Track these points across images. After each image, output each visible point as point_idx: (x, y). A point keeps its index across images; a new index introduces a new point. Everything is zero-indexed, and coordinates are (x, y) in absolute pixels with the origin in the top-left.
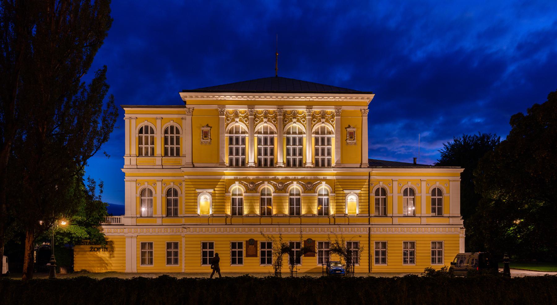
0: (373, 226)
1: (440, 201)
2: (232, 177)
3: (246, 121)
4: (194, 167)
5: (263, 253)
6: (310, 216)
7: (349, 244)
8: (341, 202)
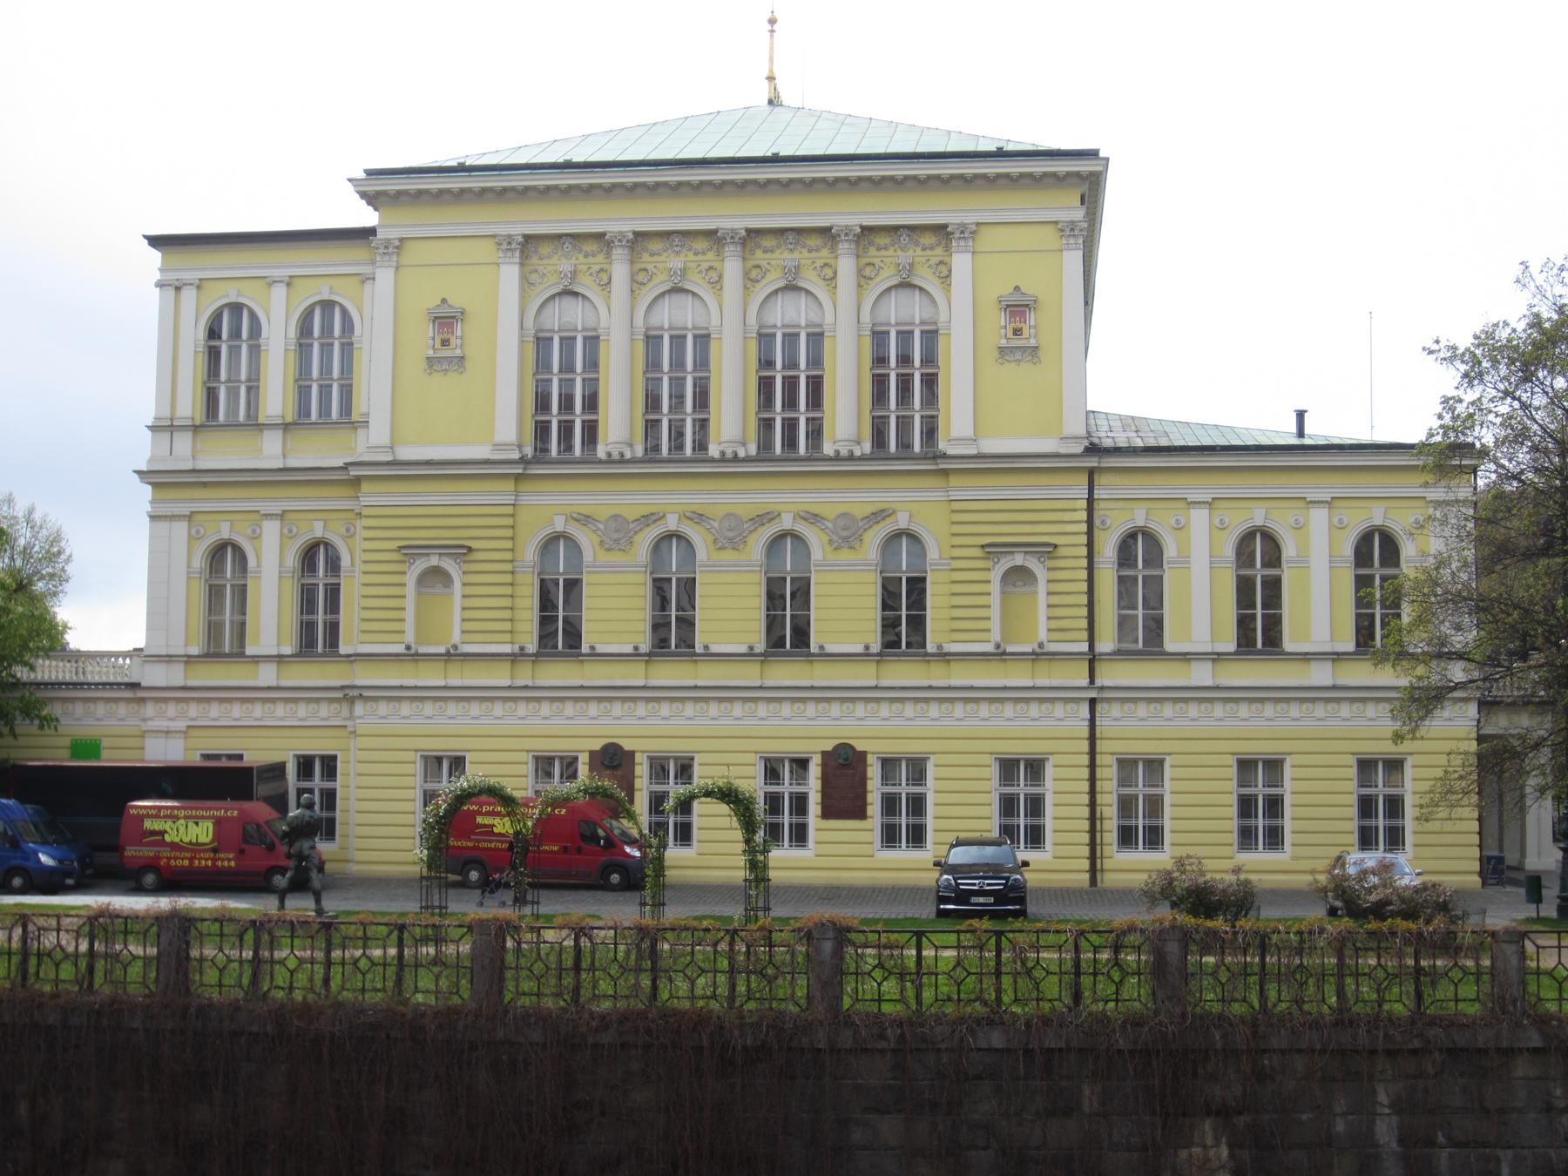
5: (890, 804)
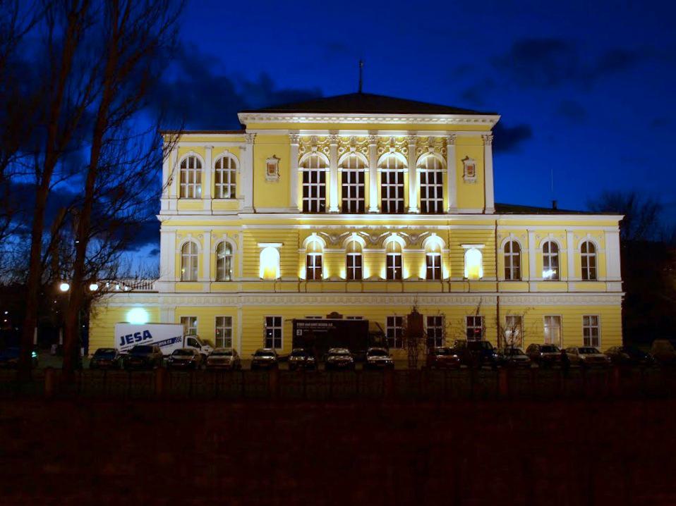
0: (503, 294)
1: (593, 260)
2: (308, 227)
3: (327, 151)
4: (255, 213)
6: (415, 280)
7: (390, 320)
8: (458, 262)
